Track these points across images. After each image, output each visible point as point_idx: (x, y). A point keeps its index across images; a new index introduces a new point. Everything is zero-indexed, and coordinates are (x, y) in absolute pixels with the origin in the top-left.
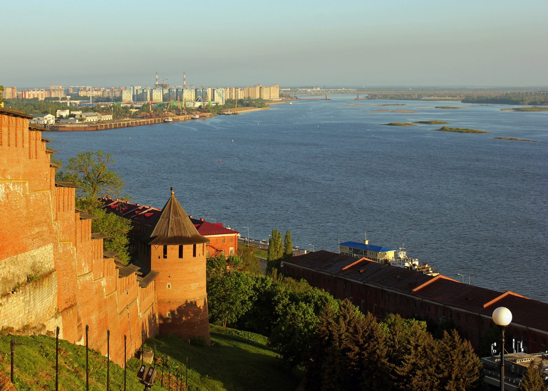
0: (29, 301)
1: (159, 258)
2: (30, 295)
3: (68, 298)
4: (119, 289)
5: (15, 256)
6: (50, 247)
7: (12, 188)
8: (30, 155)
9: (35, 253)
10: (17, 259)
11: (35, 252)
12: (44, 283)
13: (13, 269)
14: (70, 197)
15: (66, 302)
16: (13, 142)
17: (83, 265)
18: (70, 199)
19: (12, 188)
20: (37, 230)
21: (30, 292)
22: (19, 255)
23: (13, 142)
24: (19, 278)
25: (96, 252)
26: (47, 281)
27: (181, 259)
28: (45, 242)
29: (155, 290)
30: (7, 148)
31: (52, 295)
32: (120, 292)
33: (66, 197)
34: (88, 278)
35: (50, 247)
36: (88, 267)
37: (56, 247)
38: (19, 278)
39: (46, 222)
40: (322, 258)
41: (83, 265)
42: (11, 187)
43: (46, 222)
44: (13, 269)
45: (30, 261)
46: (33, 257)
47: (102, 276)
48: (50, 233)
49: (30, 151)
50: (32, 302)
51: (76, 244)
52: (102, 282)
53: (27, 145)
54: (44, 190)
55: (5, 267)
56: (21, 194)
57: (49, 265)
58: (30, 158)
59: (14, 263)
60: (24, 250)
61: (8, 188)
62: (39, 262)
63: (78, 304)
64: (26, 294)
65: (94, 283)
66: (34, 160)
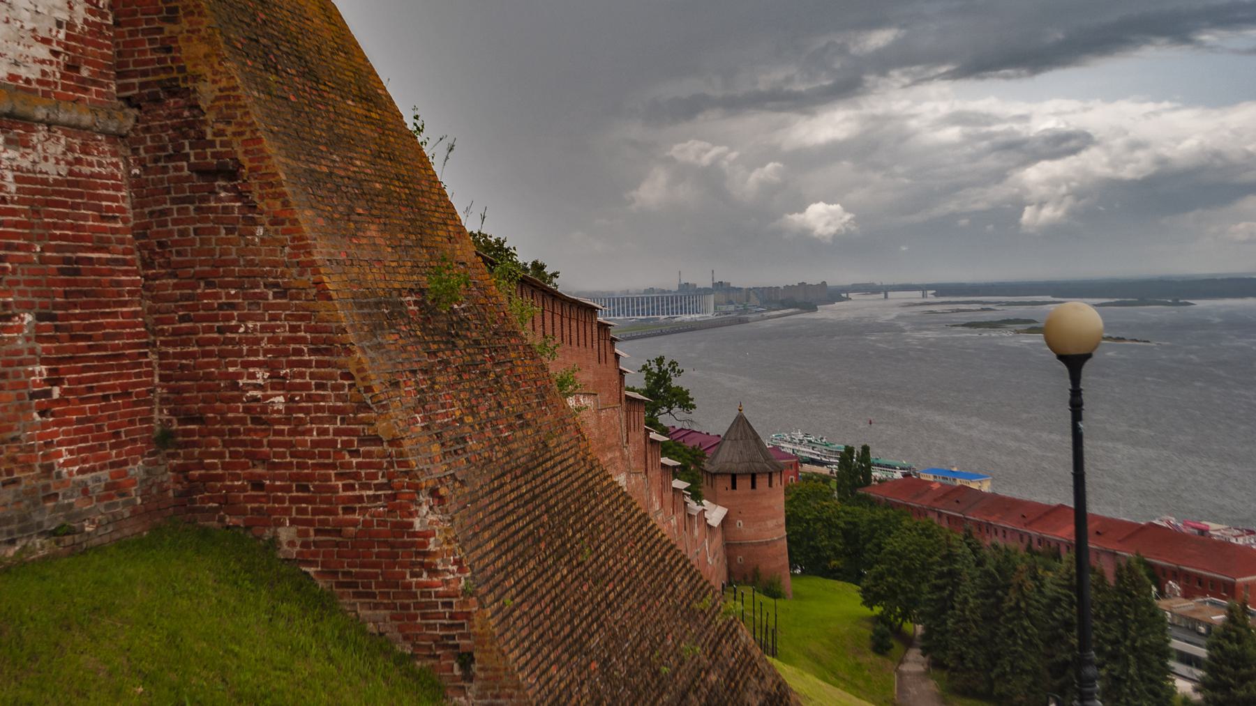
16: (582, 341)
23: (582, 341)
53: (596, 346)
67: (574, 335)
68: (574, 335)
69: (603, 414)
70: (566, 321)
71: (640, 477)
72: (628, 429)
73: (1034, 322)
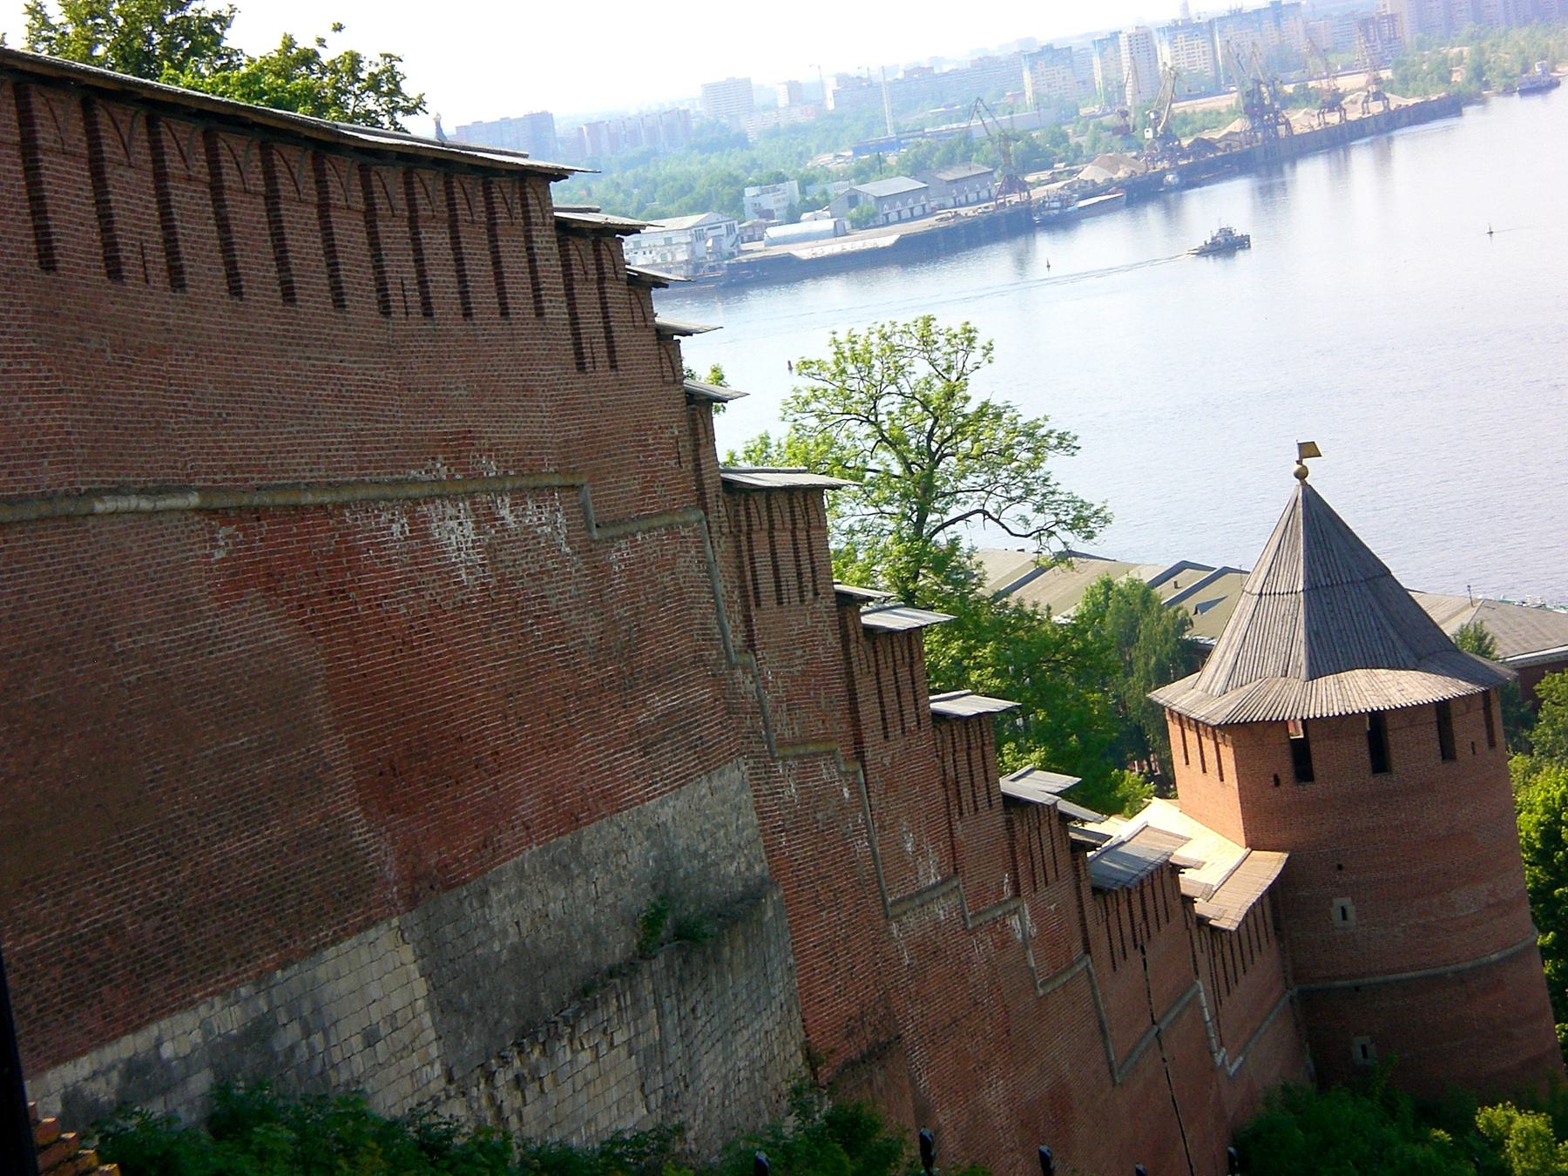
0: (662, 1046)
1: (1277, 782)
2: (661, 1016)
3: (855, 1010)
4: (1101, 946)
5: (567, 838)
6: (734, 776)
7: (510, 519)
8: (579, 354)
9: (666, 814)
10: (576, 849)
11: (667, 810)
12: (726, 951)
13: (557, 899)
14: (801, 535)
15: (850, 1034)
16: (483, 297)
17: (909, 847)
18: (803, 545)
19: (510, 519)
20: (660, 702)
21: (659, 1006)
22: (585, 830)
23: (483, 297)
24: (597, 942)
25: (965, 782)
26: (740, 941)
27: (1308, 785)
28: (708, 761)
29: (1280, 939)
30: (458, 328)
31: (775, 1005)
32: (1107, 963)
33: (783, 538)
34: (941, 910)
35: (734, 776)
36: (933, 859)
37: (762, 772)
38: (597, 942)
39: (699, 660)
40: (1214, 242)
41: (909, 847)
42: (505, 512)
43: (699, 660)
44: (557, 899)
45: (638, 855)
46: (657, 832)
47: (1008, 891)
48: (729, 710)
49: (576, 334)
50: (676, 1049)
51: (860, 756)
52: (1014, 922)
53: (556, 308)
54: (672, 511)
55: (521, 893)
56: (561, 539)
57: (740, 866)
58: (581, 367)
59: (561, 871)
60: (610, 801)
61: (492, 517)
62: (693, 853)
63: (909, 1035)
64: (642, 1013)
65: (973, 932)
66: (602, 372)
67: (442, 279)
68: (442, 279)
70: (394, 234)
72: (749, 596)
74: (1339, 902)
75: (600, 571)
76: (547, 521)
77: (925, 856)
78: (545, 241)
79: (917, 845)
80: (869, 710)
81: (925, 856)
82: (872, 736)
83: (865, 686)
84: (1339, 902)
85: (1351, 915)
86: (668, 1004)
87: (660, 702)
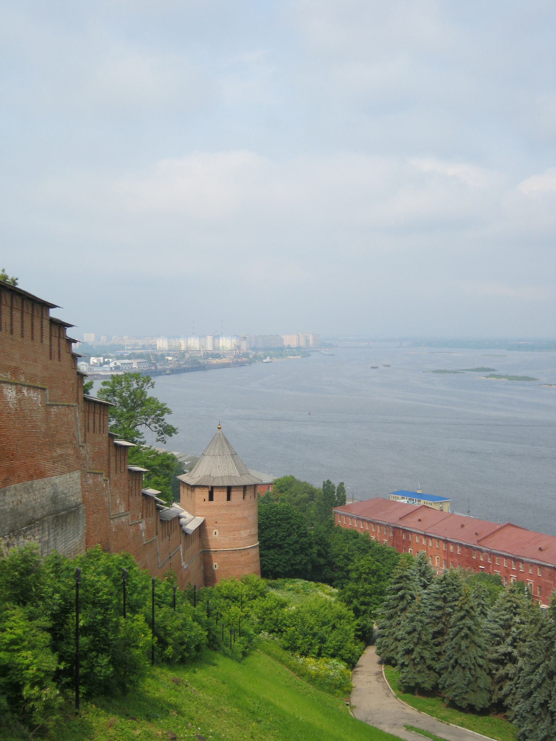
1: (205, 500)
20: (59, 451)
45: (49, 491)
53: (46, 341)
56: (39, 402)
66: (56, 361)
69: (54, 410)
71: (100, 479)
73: (493, 370)
74: (215, 531)
75: (48, 413)
76: (36, 396)
77: (121, 504)
78: (46, 323)
79: (120, 502)
80: (113, 465)
81: (121, 504)
82: (113, 472)
83: (113, 459)
84: (410, 549)
85: (217, 533)
86: (51, 531)
87: (59, 451)
